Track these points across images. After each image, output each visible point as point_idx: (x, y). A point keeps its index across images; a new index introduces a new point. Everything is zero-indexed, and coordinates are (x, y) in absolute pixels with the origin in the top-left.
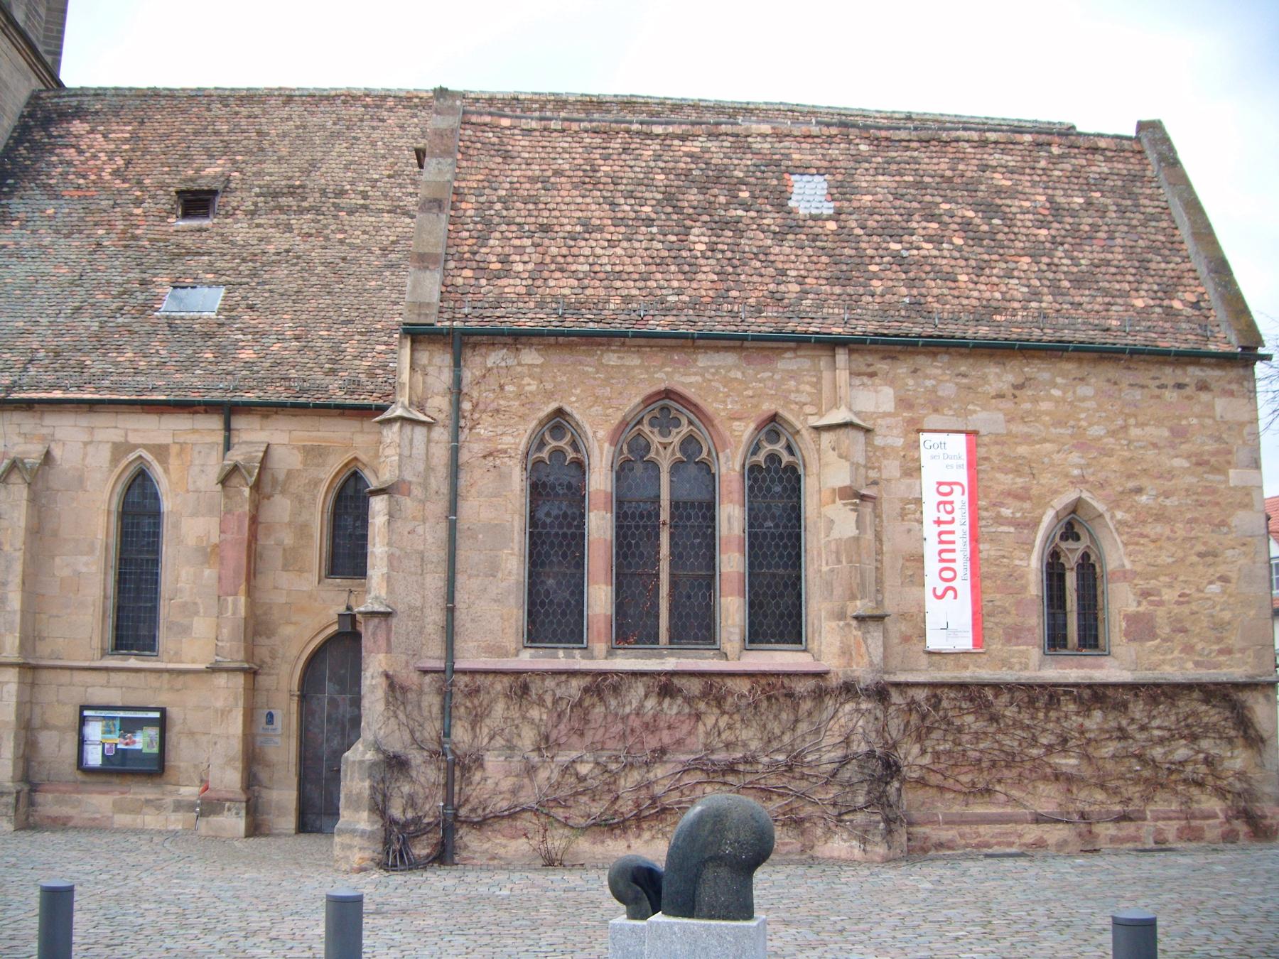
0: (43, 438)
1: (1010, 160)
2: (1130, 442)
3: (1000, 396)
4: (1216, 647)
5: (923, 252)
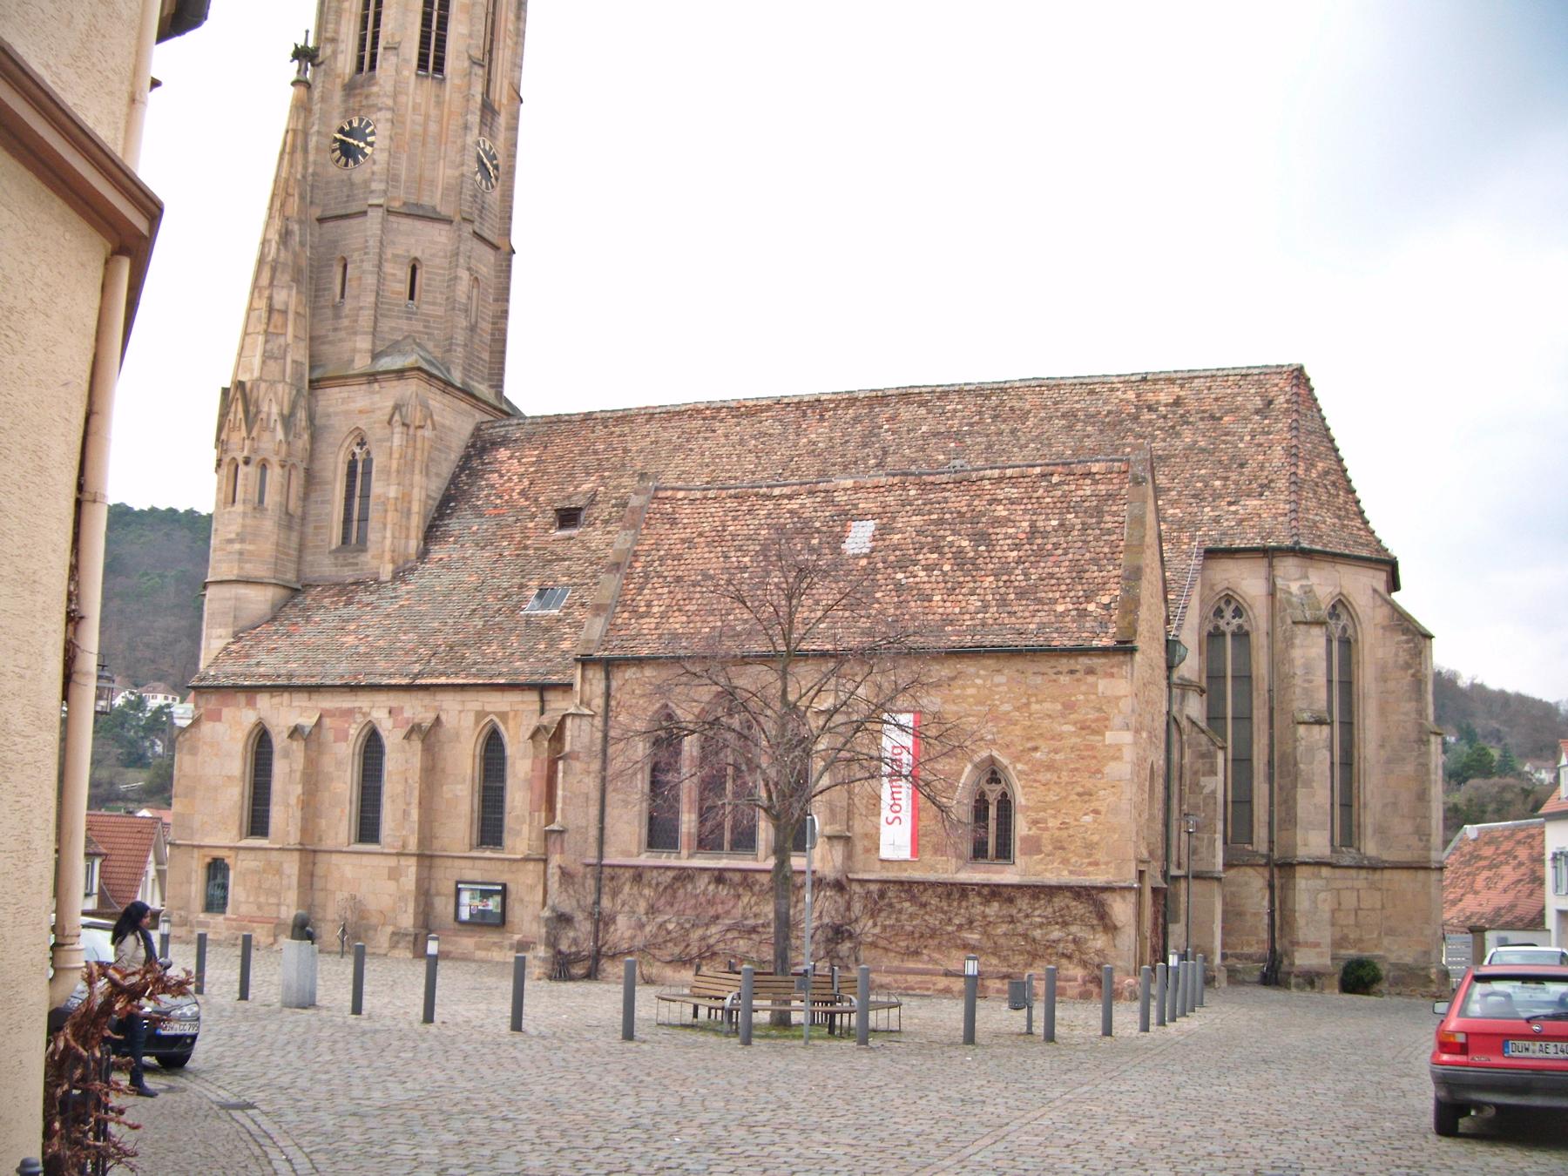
0: (436, 708)
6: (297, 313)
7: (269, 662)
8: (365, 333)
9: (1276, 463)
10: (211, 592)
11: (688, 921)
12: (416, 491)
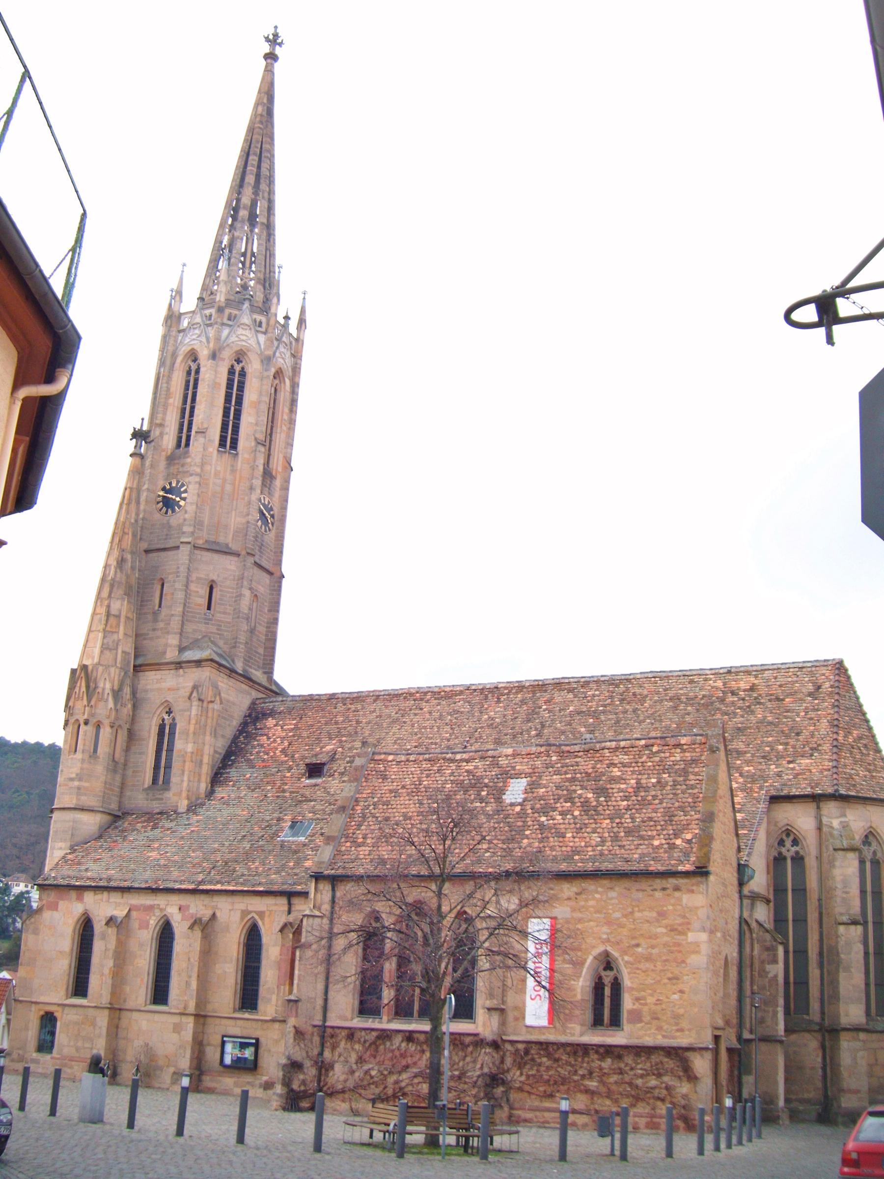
1: (625, 759)
2: (634, 920)
3: (569, 899)
4: (674, 1028)
5: (556, 822)
6: (127, 618)
7: (95, 869)
8: (175, 633)
9: (823, 732)
10: (56, 816)
11: (386, 1069)
12: (207, 747)
